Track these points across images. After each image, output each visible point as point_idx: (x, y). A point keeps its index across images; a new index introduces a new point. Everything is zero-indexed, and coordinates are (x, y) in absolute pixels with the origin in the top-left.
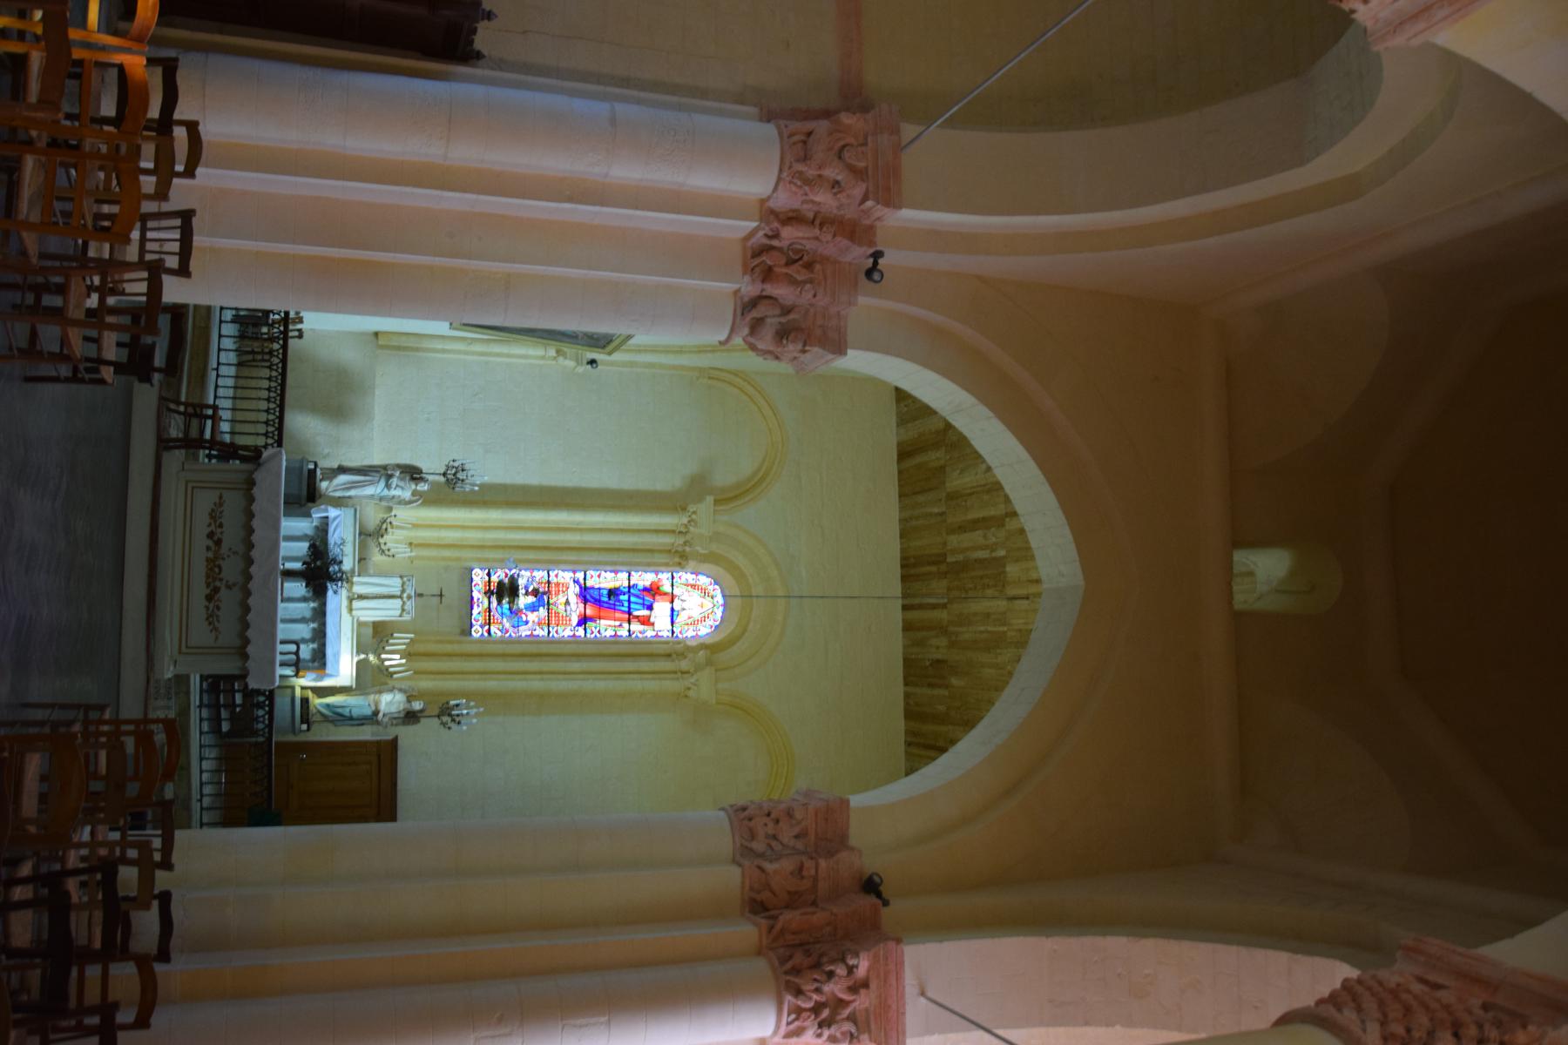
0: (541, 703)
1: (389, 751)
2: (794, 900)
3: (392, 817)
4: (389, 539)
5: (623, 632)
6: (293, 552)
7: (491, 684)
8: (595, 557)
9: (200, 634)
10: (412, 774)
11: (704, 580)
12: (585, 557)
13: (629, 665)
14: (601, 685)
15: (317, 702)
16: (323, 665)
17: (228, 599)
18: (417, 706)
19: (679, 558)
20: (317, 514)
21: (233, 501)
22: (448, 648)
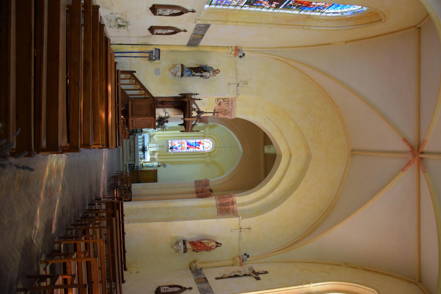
0: (180, 163)
1: (155, 172)
2: (202, 192)
3: (157, 182)
4: (154, 137)
5: (195, 150)
6: (140, 147)
7: (172, 160)
8: (189, 138)
9: (129, 158)
10: (160, 175)
11: (209, 141)
12: (187, 138)
13: (195, 156)
14: (190, 160)
15: (144, 164)
16: (145, 159)
17: (132, 154)
18: (160, 164)
19: (204, 137)
20: (143, 135)
21: (132, 141)
22: (165, 154)
